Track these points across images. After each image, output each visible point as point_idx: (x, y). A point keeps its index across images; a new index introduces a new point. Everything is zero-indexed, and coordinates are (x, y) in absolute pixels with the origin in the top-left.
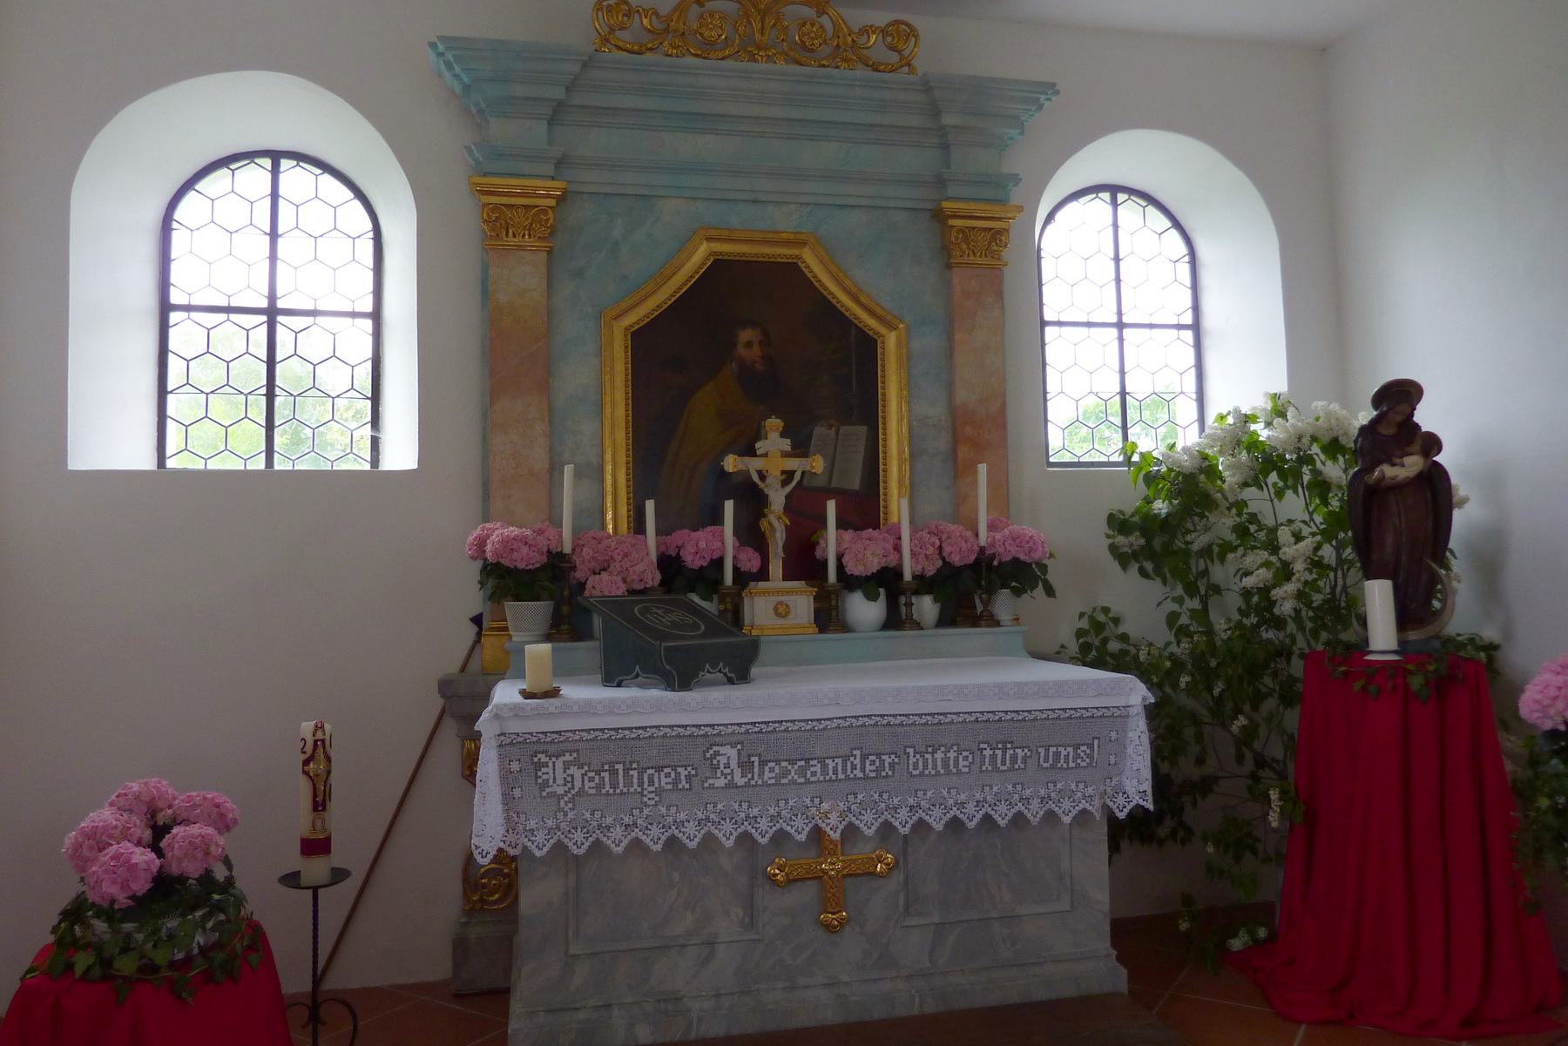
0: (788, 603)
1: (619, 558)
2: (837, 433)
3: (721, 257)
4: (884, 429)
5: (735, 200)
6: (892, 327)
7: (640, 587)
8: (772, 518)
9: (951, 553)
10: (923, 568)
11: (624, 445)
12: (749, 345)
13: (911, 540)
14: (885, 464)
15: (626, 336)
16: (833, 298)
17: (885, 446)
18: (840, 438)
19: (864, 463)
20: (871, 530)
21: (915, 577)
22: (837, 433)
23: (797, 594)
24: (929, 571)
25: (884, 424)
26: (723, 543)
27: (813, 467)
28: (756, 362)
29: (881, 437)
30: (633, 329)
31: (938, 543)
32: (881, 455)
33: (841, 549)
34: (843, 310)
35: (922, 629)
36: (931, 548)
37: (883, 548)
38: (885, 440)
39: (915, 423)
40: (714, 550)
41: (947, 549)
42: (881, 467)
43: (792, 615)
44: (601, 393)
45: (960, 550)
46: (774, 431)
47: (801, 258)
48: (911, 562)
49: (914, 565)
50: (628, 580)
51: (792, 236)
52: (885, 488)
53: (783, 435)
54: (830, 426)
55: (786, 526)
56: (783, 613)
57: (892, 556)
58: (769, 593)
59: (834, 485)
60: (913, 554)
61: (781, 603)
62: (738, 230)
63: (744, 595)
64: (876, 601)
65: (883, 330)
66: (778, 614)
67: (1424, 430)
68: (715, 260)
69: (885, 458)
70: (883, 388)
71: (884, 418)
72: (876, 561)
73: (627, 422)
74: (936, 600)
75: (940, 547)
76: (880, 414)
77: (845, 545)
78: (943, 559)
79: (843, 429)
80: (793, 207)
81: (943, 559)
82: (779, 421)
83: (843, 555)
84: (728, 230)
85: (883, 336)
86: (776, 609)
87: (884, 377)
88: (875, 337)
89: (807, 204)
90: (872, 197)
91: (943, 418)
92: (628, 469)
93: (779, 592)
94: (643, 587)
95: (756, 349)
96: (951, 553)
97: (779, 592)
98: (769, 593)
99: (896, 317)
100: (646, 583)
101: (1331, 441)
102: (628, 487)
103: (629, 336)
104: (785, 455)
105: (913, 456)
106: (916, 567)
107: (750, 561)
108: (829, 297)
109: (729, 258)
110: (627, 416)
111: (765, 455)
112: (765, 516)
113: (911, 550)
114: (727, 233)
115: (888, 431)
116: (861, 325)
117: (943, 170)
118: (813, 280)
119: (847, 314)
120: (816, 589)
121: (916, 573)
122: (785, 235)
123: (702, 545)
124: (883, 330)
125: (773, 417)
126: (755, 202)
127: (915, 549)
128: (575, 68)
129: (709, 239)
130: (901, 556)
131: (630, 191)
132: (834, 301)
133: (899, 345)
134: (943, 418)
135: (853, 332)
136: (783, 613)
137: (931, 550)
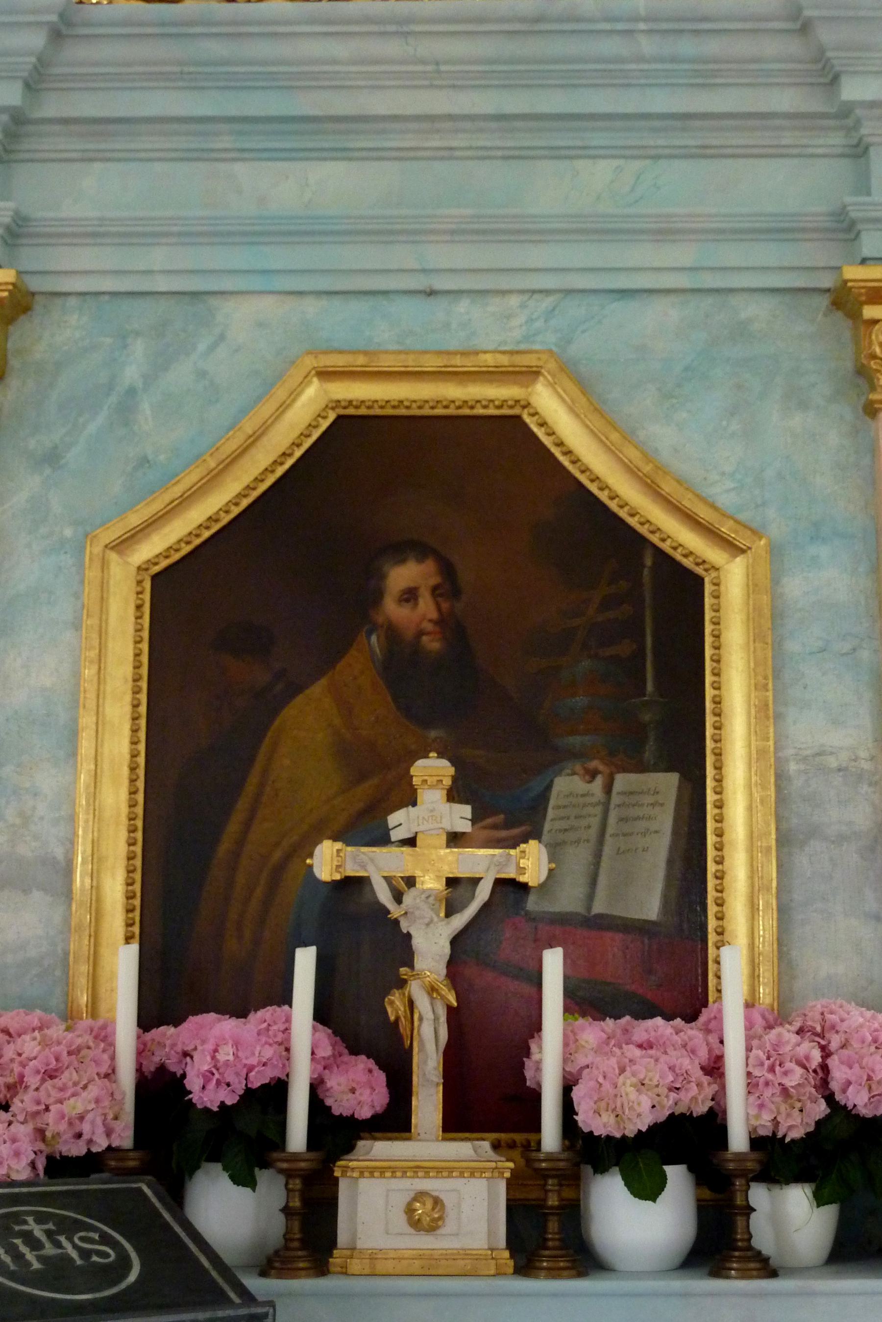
0: (442, 1196)
1: (33, 1081)
2: (608, 789)
3: (351, 411)
4: (719, 780)
5: (385, 293)
6: (735, 549)
7: (78, 1150)
8: (416, 989)
9: (849, 1083)
10: (775, 1122)
11: (124, 820)
12: (410, 596)
13: (749, 1049)
14: (720, 861)
15: (139, 583)
16: (612, 498)
17: (719, 819)
18: (615, 799)
19: (670, 862)
20: (659, 1020)
21: (757, 1142)
22: (608, 789)
23: (461, 1175)
24: (790, 1128)
25: (718, 768)
26: (288, 1050)
27: (522, 870)
28: (423, 634)
29: (710, 797)
30: (157, 569)
31: (816, 1056)
32: (711, 839)
33: (572, 1068)
34: (623, 514)
35: (772, 1273)
36: (799, 1071)
37: (672, 1068)
38: (719, 805)
39: (793, 767)
40: (251, 1069)
41: (839, 1073)
42: (711, 868)
43: (449, 1226)
44: (75, 704)
45: (869, 1078)
46: (432, 787)
47: (527, 405)
48: (747, 1105)
49: (753, 1112)
50: (48, 1134)
51: (504, 360)
52: (720, 918)
53: (453, 795)
54: (592, 775)
55: (450, 1009)
56: (426, 1220)
57: (694, 1090)
58: (393, 1171)
59: (599, 908)
60: (752, 1085)
61: (420, 1196)
62: (386, 352)
63: (337, 1173)
64: (654, 1200)
65: (713, 554)
66: (416, 1224)
67: (190, 1017)
68: (340, 418)
69: (719, 848)
70: (717, 687)
71: (718, 754)
72: (645, 1102)
73: (133, 769)
74: (820, 1200)
75: (825, 1068)
76: (709, 744)
77: (581, 1060)
78: (830, 1099)
79: (622, 781)
80: (514, 301)
81: (830, 1099)
82: (445, 763)
83: (576, 1083)
84: (366, 353)
85: (717, 569)
86: (410, 1211)
87: (718, 661)
88: (699, 570)
89: (547, 292)
90: (691, 269)
91: (863, 754)
92: (130, 871)
93: (418, 1169)
94: (83, 1151)
95: (426, 607)
96: (849, 1083)
97: (418, 1169)
98: (393, 1171)
99: (746, 527)
100: (90, 1141)
101: (580, 1177)
102: (129, 910)
103: (148, 585)
104: (455, 839)
105: (784, 840)
106: (758, 1117)
107: (353, 1091)
108: (593, 488)
109: (371, 412)
110: (134, 755)
111: (411, 842)
112: (402, 983)
113: (749, 1074)
114: (361, 360)
115: (728, 784)
116: (666, 547)
117: (848, 199)
118: (556, 452)
119: (633, 522)
120: (511, 1165)
121: (762, 1132)
122: (489, 359)
123: (226, 1054)
124: (713, 554)
125: (433, 754)
126: (431, 293)
127: (757, 1072)
128: (37, 40)
129: (325, 375)
130: (723, 1087)
131: (162, 284)
132: (603, 496)
133: (752, 587)
134: (863, 754)
135: (648, 561)
136: (426, 1220)
137: (795, 1077)
